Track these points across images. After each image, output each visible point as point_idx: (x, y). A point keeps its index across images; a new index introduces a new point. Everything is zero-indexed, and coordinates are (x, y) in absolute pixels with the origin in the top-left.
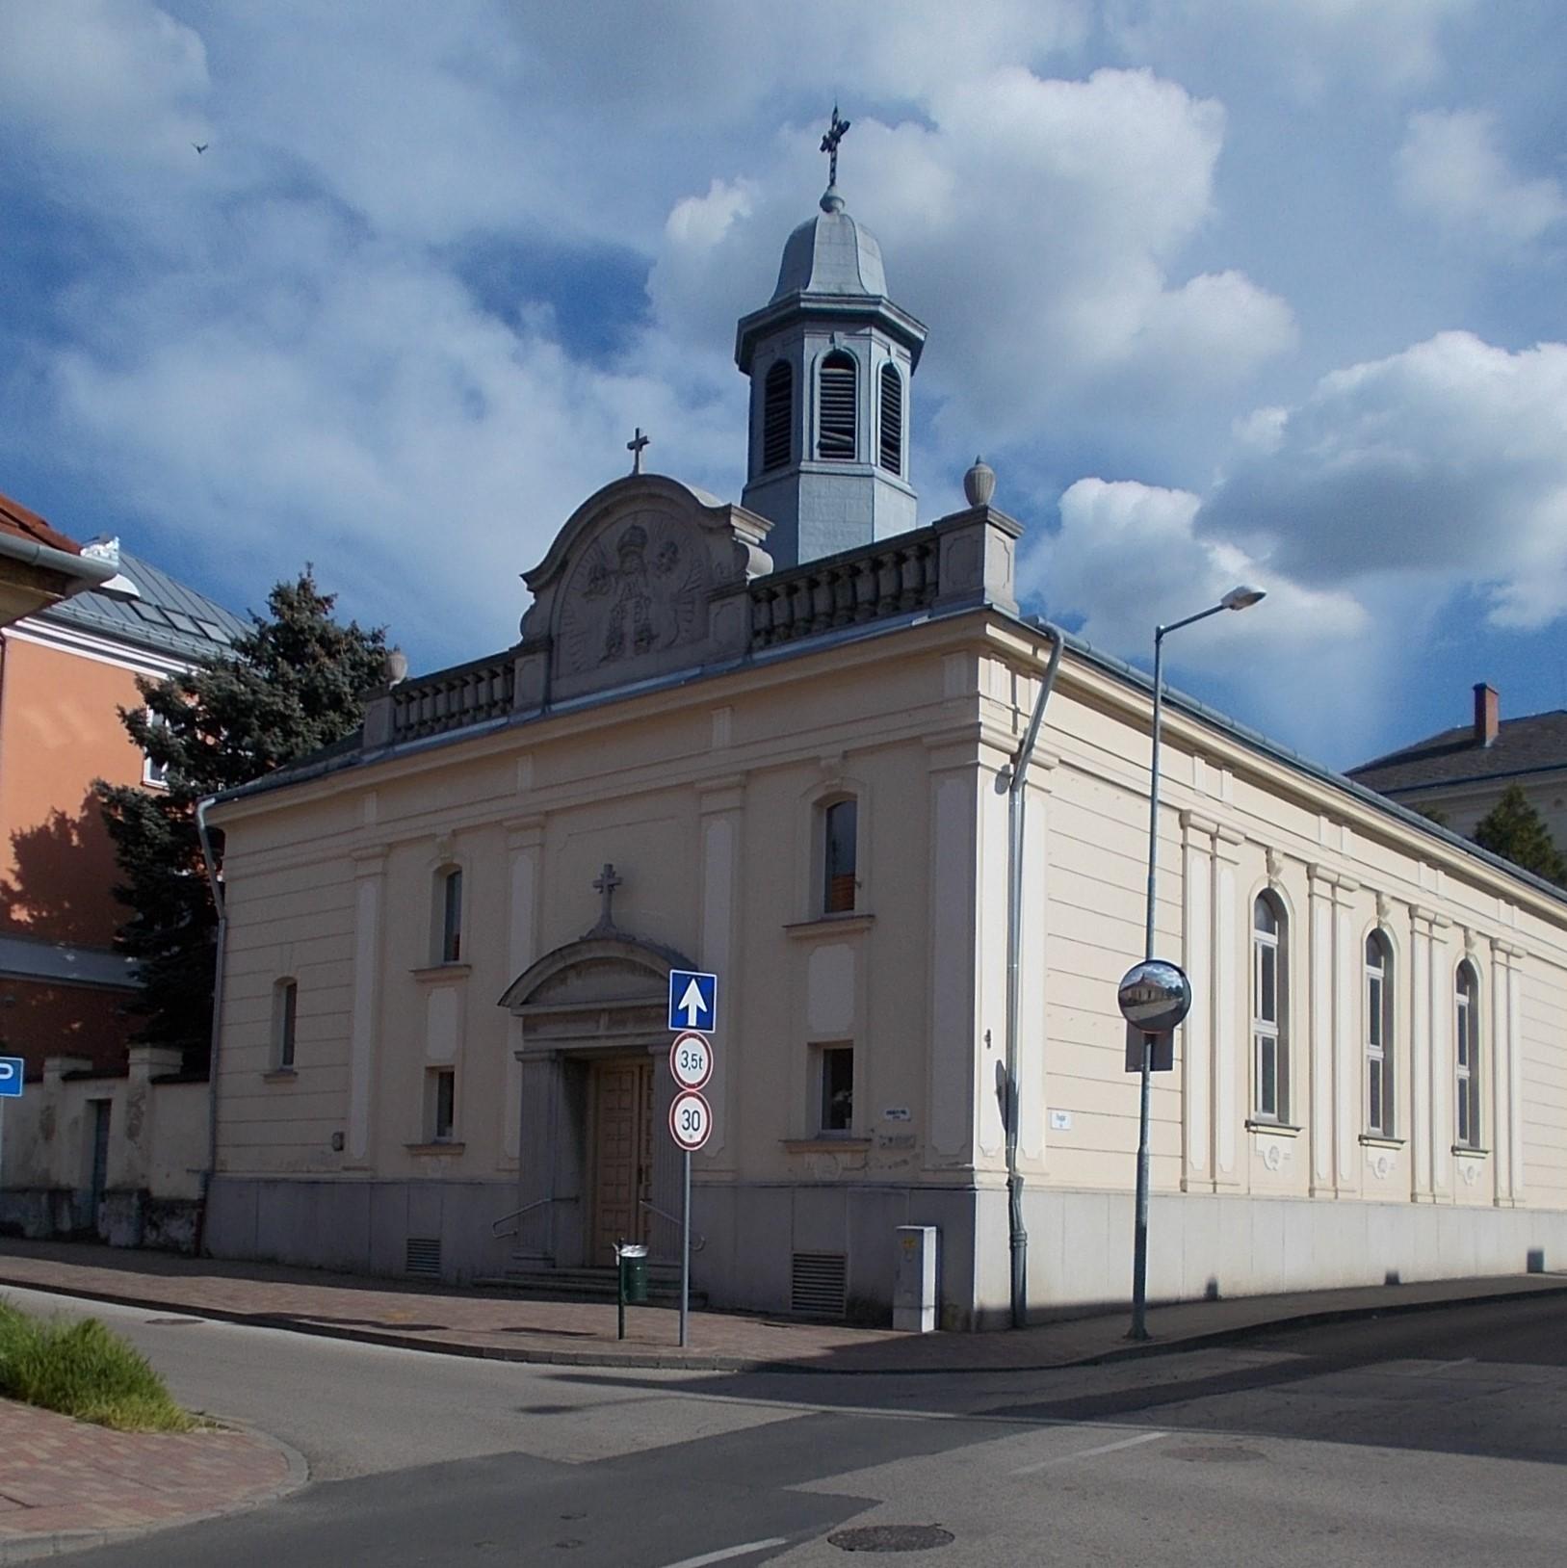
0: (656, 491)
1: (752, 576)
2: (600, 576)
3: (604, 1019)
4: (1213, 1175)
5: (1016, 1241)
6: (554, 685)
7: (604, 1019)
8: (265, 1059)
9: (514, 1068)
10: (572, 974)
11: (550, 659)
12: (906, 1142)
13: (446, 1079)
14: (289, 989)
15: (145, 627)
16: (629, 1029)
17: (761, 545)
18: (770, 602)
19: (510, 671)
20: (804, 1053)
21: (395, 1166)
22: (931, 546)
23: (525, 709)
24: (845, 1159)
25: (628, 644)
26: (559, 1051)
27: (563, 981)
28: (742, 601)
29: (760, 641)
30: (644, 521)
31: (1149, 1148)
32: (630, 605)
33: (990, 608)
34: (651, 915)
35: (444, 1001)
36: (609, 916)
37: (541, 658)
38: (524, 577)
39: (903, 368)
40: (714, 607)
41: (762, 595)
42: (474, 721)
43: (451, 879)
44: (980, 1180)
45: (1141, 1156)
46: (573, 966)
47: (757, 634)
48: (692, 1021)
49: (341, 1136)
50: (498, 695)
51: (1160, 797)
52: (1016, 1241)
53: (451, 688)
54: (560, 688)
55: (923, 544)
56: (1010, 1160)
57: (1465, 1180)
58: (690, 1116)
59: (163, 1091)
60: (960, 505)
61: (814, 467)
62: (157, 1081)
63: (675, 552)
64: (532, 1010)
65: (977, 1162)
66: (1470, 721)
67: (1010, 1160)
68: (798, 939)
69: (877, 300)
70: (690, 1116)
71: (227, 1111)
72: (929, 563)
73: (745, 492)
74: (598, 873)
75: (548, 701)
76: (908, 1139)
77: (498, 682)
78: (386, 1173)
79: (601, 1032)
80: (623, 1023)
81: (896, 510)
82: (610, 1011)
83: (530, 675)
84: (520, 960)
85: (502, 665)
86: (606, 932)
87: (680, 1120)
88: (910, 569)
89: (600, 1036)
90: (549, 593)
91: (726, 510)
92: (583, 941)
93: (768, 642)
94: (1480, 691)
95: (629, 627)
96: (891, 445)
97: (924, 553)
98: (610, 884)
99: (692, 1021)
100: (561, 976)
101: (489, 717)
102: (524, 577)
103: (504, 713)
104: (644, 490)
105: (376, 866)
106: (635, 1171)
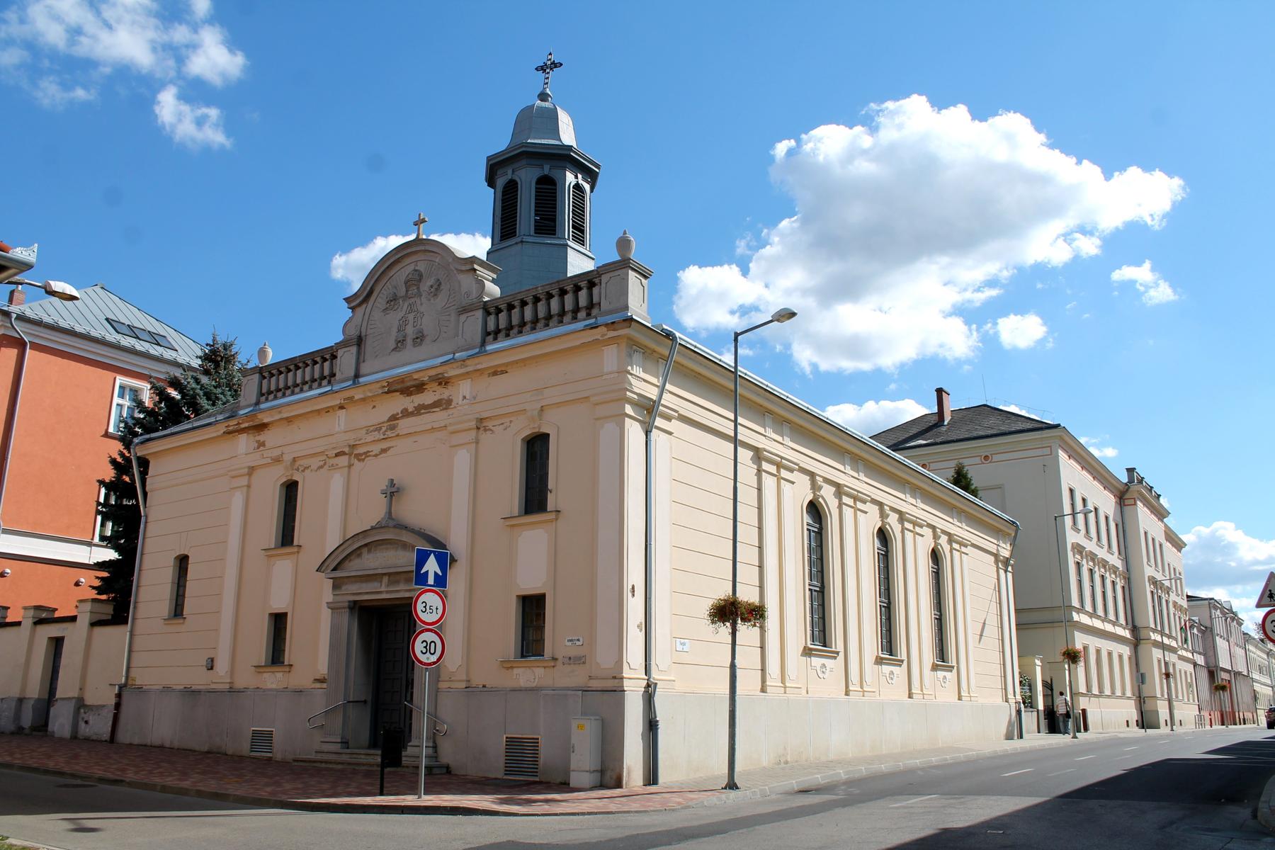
0: (428, 248)
1: (486, 299)
2: (393, 299)
3: (385, 579)
4: (783, 681)
5: (651, 726)
6: (362, 365)
7: (385, 579)
8: (165, 607)
9: (326, 614)
10: (365, 550)
11: (359, 353)
12: (579, 660)
13: (279, 621)
14: (183, 561)
15: (119, 337)
16: (402, 587)
17: (493, 281)
18: (497, 315)
19: (334, 357)
20: (267, 616)
21: (246, 679)
22: (597, 281)
23: (343, 381)
24: (539, 672)
25: (409, 341)
26: (355, 602)
27: (359, 555)
28: (479, 314)
29: (491, 337)
30: (421, 267)
31: (737, 662)
32: (411, 317)
33: (631, 319)
34: (415, 511)
35: (284, 567)
36: (390, 513)
37: (354, 349)
38: (347, 300)
39: (587, 187)
40: (463, 317)
41: (492, 310)
42: (311, 388)
43: (291, 490)
44: (627, 685)
45: (733, 667)
46: (366, 545)
47: (489, 334)
48: (431, 580)
49: (212, 660)
50: (326, 372)
51: (739, 437)
52: (651, 726)
53: (297, 368)
54: (364, 368)
55: (590, 280)
56: (647, 670)
57: (939, 688)
58: (428, 646)
59: (99, 631)
60: (615, 257)
61: (1085, 619)
62: (94, 624)
63: (439, 285)
64: (338, 574)
65: (626, 673)
66: (935, 410)
67: (647, 670)
68: (513, 526)
69: (570, 148)
70: (428, 646)
71: (138, 641)
72: (595, 290)
73: (488, 253)
74: (384, 485)
75: (357, 376)
76: (580, 658)
77: (327, 364)
78: (240, 683)
79: (383, 589)
80: (397, 582)
81: (578, 263)
82: (389, 574)
83: (346, 361)
84: (332, 541)
85: (329, 355)
86: (392, 522)
87: (419, 647)
88: (583, 295)
89: (382, 592)
90: (360, 311)
91: (473, 260)
92: (373, 528)
93: (495, 339)
94: (940, 392)
95: (410, 330)
96: (579, 229)
97: (591, 285)
98: (393, 492)
99: (431, 580)
100: (357, 552)
101: (320, 386)
102: (347, 300)
103: (329, 382)
104: (422, 248)
105: (244, 481)
106: (404, 683)
